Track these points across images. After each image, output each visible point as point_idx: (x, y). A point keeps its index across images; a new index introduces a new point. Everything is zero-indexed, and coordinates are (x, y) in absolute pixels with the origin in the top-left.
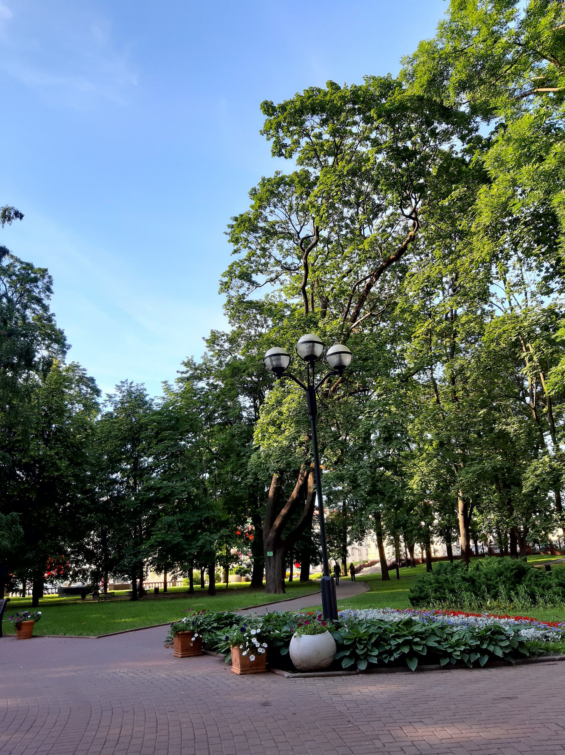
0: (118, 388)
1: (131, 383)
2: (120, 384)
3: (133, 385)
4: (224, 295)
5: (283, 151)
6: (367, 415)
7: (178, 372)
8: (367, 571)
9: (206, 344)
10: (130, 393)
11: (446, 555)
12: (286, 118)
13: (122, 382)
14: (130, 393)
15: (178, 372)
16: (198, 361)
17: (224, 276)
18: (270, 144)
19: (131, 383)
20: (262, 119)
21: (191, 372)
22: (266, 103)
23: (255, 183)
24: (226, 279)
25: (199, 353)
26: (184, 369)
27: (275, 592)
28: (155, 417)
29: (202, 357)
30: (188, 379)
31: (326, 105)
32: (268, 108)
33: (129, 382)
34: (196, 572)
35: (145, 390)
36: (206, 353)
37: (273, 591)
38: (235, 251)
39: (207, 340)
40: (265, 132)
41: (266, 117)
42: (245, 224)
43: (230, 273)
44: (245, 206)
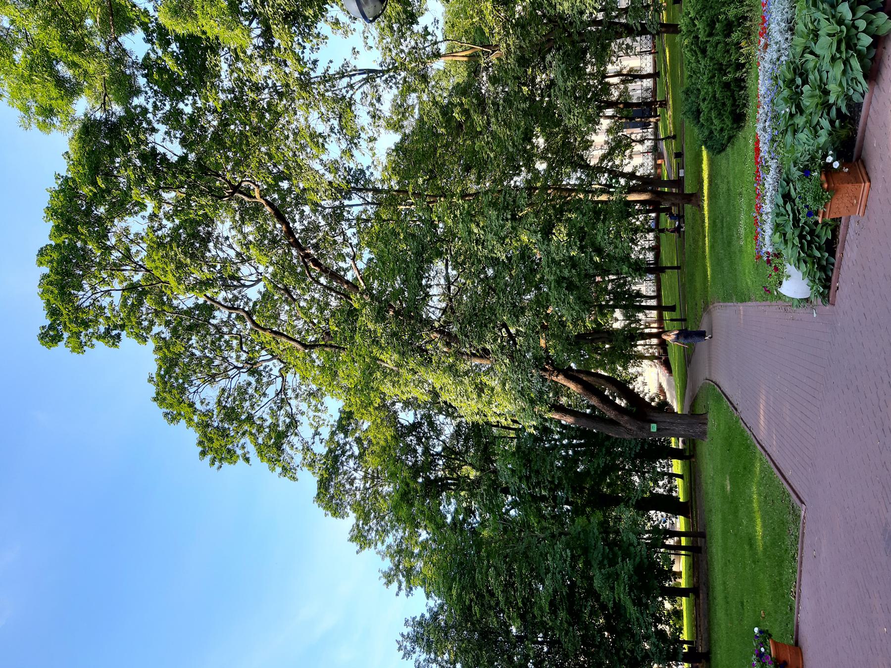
0: (407, 655)
1: (403, 635)
2: (402, 653)
3: (405, 634)
4: (299, 474)
7: (397, 595)
9: (367, 549)
10: (416, 639)
11: (652, 277)
12: (67, 318)
13: (400, 649)
14: (416, 639)
15: (397, 595)
16: (387, 564)
17: (273, 470)
18: (100, 345)
19: (403, 635)
20: (61, 349)
21: (401, 577)
22: (43, 337)
23: (157, 411)
24: (279, 470)
25: (375, 560)
26: (395, 585)
27: (706, 424)
28: (454, 592)
29: (383, 559)
30: (408, 581)
31: (66, 271)
32: (50, 336)
33: (400, 639)
34: (665, 568)
35: (414, 619)
36: (379, 553)
37: (703, 427)
38: (247, 460)
40: (80, 347)
41: (61, 344)
42: (217, 444)
43: (273, 461)
44: (187, 436)
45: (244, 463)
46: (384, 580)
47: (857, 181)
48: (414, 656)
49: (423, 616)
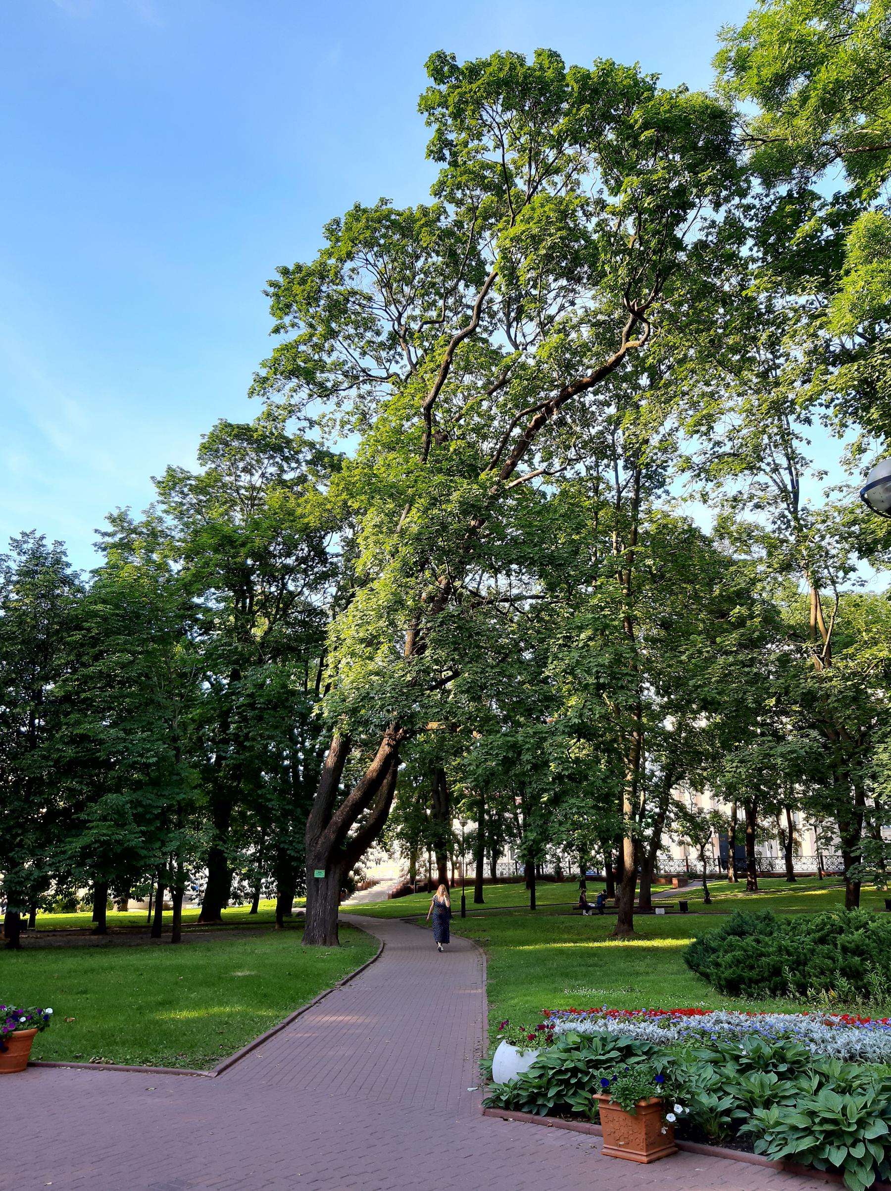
0: (16, 544)
1: (42, 538)
2: (19, 537)
4: (258, 400)
5: (447, 152)
6: (561, 642)
7: (96, 531)
8: (363, 897)
10: (37, 556)
12: (464, 90)
13: (24, 534)
14: (37, 556)
15: (96, 531)
16: (137, 518)
18: (430, 133)
19: (42, 538)
22: (441, 57)
23: (342, 210)
24: (263, 373)
25: (141, 501)
26: (110, 528)
27: (324, 943)
28: (99, 607)
29: (144, 512)
30: (114, 546)
31: (530, 88)
33: (38, 535)
35: (64, 553)
36: (153, 506)
38: (277, 330)
39: (159, 482)
40: (427, 107)
41: (431, 82)
43: (274, 365)
44: (309, 251)
45: (272, 327)
46: (115, 513)
47: (649, 1146)
48: (14, 554)
49: (68, 565)
